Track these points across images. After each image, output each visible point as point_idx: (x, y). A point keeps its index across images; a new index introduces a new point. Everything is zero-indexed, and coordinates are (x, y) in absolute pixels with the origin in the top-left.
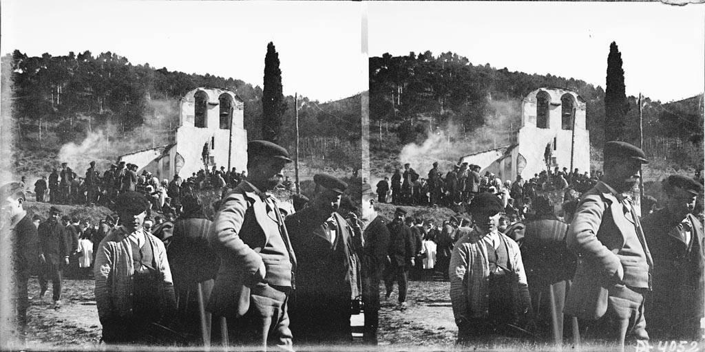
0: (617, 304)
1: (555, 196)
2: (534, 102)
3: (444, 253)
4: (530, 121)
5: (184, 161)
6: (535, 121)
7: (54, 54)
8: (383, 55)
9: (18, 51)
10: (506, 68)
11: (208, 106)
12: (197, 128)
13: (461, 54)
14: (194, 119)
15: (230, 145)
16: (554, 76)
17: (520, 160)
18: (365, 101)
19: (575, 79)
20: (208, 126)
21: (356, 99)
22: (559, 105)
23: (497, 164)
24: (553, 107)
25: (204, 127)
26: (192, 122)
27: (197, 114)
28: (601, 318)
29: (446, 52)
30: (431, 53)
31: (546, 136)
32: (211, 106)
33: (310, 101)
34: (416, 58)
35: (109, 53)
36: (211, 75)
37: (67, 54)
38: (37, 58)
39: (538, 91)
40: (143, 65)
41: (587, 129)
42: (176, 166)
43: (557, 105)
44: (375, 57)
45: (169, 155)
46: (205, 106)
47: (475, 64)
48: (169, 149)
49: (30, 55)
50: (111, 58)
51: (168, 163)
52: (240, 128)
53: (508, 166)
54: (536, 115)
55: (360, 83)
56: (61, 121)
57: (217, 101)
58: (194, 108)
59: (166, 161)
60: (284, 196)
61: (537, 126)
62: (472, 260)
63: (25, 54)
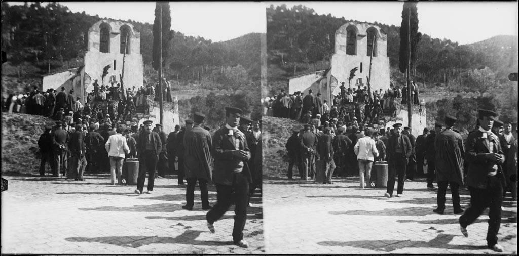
2: (97, 31)
3: (509, 191)
10: (97, 15)
11: (358, 38)
12: (101, 53)
14: (99, 46)
17: (332, 80)
20: (358, 54)
24: (360, 37)
25: (108, 52)
26: (344, 50)
27: (348, 44)
31: (107, 59)
32: (113, 35)
42: (330, 87)
43: (116, 34)
45: (327, 78)
46: (109, 35)
47: (320, 14)
52: (385, 56)
53: (324, 86)
54: (99, 42)
58: (346, 39)
61: (100, 51)
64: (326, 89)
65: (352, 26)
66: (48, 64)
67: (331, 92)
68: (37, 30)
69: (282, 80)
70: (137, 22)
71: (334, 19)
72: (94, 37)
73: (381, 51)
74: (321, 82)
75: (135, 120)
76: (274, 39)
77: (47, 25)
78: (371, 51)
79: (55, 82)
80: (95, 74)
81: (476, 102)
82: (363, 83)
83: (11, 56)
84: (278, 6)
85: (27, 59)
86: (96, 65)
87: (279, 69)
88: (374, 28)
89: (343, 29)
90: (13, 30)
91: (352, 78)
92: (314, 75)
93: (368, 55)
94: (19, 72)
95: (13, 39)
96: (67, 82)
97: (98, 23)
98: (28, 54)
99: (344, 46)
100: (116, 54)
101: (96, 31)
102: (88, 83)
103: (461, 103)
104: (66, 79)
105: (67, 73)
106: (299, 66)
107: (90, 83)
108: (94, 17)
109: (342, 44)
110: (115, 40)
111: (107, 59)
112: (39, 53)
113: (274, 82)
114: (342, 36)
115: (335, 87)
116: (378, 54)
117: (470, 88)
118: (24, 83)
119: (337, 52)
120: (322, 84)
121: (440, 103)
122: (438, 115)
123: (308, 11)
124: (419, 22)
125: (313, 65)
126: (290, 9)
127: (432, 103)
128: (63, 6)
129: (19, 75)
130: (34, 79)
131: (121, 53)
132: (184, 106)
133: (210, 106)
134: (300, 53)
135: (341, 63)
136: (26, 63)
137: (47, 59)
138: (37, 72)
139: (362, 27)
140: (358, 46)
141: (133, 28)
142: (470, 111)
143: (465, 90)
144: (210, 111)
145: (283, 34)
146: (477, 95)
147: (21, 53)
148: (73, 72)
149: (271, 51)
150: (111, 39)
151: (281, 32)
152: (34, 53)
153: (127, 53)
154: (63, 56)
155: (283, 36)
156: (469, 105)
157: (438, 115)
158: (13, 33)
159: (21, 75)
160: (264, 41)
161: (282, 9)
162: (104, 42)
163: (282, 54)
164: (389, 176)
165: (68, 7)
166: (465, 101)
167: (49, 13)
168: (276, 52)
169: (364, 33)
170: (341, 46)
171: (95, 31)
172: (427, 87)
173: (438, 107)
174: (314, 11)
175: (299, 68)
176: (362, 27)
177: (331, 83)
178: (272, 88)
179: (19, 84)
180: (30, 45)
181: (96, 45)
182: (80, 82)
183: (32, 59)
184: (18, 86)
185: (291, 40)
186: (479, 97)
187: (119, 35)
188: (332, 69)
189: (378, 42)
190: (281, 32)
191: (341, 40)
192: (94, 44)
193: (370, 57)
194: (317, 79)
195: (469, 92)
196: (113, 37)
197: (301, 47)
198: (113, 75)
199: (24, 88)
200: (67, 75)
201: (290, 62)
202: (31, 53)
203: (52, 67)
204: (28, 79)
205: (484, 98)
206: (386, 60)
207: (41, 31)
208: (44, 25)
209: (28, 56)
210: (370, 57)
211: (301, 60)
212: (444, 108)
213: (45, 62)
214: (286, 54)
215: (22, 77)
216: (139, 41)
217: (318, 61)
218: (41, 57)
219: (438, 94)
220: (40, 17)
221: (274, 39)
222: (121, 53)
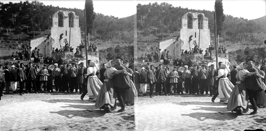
0: (232, 117)
1: (62, 54)
2: (57, 16)
4: (185, 26)
5: (54, 40)
11: (64, 18)
16: (77, 9)
18: (135, 18)
20: (193, 28)
21: (133, 16)
24: (65, 18)
26: (186, 27)
27: (59, 21)
31: (192, 32)
32: (194, 20)
36: (76, 8)
43: (66, 17)
45: (49, 39)
47: (175, 7)
50: (165, 5)
55: (134, 12)
60: (93, 54)
62: (265, 86)
64: (178, 46)
65: (61, 12)
66: (33, 33)
67: (180, 48)
68: (28, 15)
69: (156, 42)
71: (183, 9)
72: (55, 19)
74: (175, 43)
75: (206, 63)
76: (152, 21)
77: (32, 13)
78: (200, 26)
79: (36, 43)
80: (186, 40)
81: (127, 49)
82: (67, 41)
83: (15, 29)
84: (24, 2)
85: (23, 31)
87: (155, 37)
88: (73, 13)
89: (186, 16)
90: (15, 16)
91: (190, 41)
92: (172, 40)
94: (147, 39)
95: (15, 21)
96: (42, 43)
97: (186, 13)
98: (152, 30)
99: (57, 22)
101: (56, 16)
102: (53, 43)
103: (248, 51)
104: (171, 43)
105: (42, 38)
106: (165, 35)
107: (54, 43)
108: (56, 7)
109: (56, 22)
110: (195, 22)
111: (192, 32)
112: (28, 27)
113: (152, 43)
114: (185, 19)
116: (75, 26)
117: (124, 41)
118: (21, 43)
119: (183, 27)
121: (238, 52)
122: (107, 56)
123: (40, 4)
124: (94, 9)
125: (43, 32)
126: (31, 3)
127: (104, 50)
128: (40, 2)
129: (19, 39)
130: (26, 41)
132: (103, 53)
133: (117, 53)
134: (165, 28)
135: (185, 33)
136: (22, 33)
137: (33, 30)
138: (157, 39)
139: (66, 12)
141: (204, 15)
142: (253, 55)
143: (122, 42)
144: (247, 57)
145: (156, 18)
146: (257, 47)
147: (20, 28)
148: (175, 39)
149: (22, 25)
150: (64, 20)
151: (26, 15)
152: (155, 30)
153: (201, 28)
154: (170, 30)
155: (27, 17)
156: (253, 52)
157: (107, 56)
158: (15, 18)
159: (20, 40)
161: (156, 5)
162: (60, 22)
163: (156, 29)
164: (232, 82)
165: (157, 2)
166: (251, 50)
167: (33, 7)
168: (152, 28)
169: (67, 16)
170: (56, 23)
171: (185, 18)
172: (102, 42)
173: (237, 54)
174: (172, 5)
175: (165, 36)
176: (66, 12)
177: (51, 42)
178: (151, 47)
179: (19, 44)
180: (24, 24)
181: (57, 23)
182: (49, 42)
183: (25, 31)
184: (18, 45)
185: (160, 21)
186: (129, 46)
187: (197, 20)
188: (51, 35)
189: (75, 20)
190: (26, 15)
191: (185, 21)
194: (44, 40)
195: (124, 43)
196: (194, 21)
197: (166, 24)
198: (195, 40)
199: (150, 48)
200: (42, 40)
201: (161, 32)
202: (24, 28)
203: (36, 35)
204: (24, 41)
205: (261, 48)
207: (158, 18)
208: (30, 13)
209: (152, 31)
211: (166, 31)
212: (110, 52)
213: (32, 32)
214: (29, 27)
215: (20, 41)
216: (208, 22)
217: (46, 30)
218: (158, 32)
219: (236, 47)
220: (29, 9)
221: (152, 21)
222: (198, 28)
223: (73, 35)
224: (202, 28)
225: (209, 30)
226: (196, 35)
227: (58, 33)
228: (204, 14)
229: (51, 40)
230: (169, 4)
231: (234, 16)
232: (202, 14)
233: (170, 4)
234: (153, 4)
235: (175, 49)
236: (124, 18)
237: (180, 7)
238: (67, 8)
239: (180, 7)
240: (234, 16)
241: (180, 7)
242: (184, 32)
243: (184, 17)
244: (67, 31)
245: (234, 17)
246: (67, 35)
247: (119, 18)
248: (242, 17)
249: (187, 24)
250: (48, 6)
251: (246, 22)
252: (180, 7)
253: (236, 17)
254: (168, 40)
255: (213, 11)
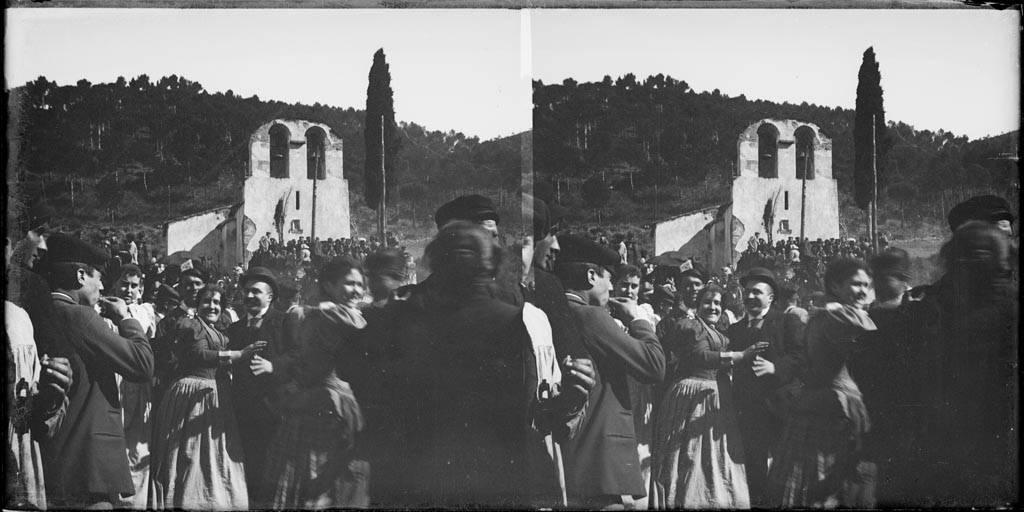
6: (267, 168)
7: (581, 80)
8: (565, 81)
9: (44, 78)
12: (762, 179)
13: (191, 77)
14: (269, 166)
15: (803, 202)
17: (246, 224)
19: (843, 109)
20: (291, 175)
21: (516, 139)
22: (791, 143)
23: (218, 232)
25: (773, 177)
26: (754, 170)
28: (323, 492)
29: (654, 75)
30: (148, 78)
33: (466, 137)
34: (614, 84)
35: (174, 77)
37: (601, 80)
38: (557, 85)
39: (272, 123)
40: (710, 91)
41: (345, 178)
44: (553, 85)
45: (236, 220)
47: (211, 92)
48: (724, 211)
49: (60, 84)
51: (723, 232)
52: (829, 178)
53: (719, 234)
55: (515, 118)
56: (590, 176)
57: (302, 138)
58: (269, 150)
59: (720, 228)
61: (271, 176)
63: (54, 82)
70: (331, 107)
73: (822, 169)
74: (713, 228)
82: (790, 228)
86: (265, 202)
93: (308, 178)
99: (753, 161)
100: (789, 179)
101: (752, 139)
107: (742, 235)
114: (750, 145)
115: (251, 236)
119: (742, 173)
120: (716, 231)
131: (798, 177)
140: (290, 161)
160: (527, 152)
174: (200, 87)
177: (732, 230)
181: (752, 166)
192: (749, 163)
193: (801, 181)
198: (783, 219)
200: (697, 221)
206: (832, 185)
210: (801, 181)
222: (798, 177)
223: (321, 207)
224: (321, 176)
225: (344, 185)
226: (300, 200)
227: (270, 199)
228: (818, 126)
229: (731, 225)
230: (676, 81)
231: (431, 128)
232: (321, 125)
233: (194, 81)
234: (619, 78)
235: (225, 246)
236: (992, 139)
237: (717, 91)
238: (776, 103)
239: (717, 91)
240: (919, 127)
241: (717, 91)
242: (746, 191)
243: (260, 137)
244: (300, 194)
245: (427, 129)
246: (301, 207)
247: (480, 142)
248: (946, 131)
249: (269, 160)
250: (219, 93)
251: (474, 149)
252: (717, 91)
253: (926, 131)
254: (688, 218)
255: (852, 110)
